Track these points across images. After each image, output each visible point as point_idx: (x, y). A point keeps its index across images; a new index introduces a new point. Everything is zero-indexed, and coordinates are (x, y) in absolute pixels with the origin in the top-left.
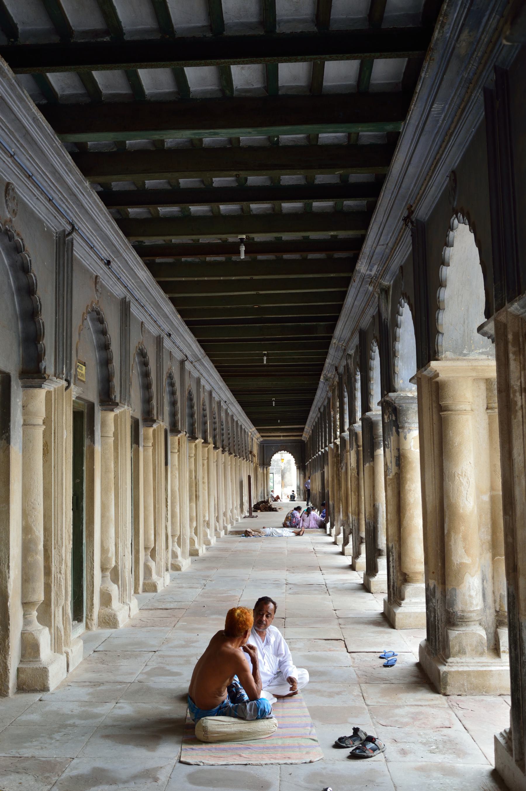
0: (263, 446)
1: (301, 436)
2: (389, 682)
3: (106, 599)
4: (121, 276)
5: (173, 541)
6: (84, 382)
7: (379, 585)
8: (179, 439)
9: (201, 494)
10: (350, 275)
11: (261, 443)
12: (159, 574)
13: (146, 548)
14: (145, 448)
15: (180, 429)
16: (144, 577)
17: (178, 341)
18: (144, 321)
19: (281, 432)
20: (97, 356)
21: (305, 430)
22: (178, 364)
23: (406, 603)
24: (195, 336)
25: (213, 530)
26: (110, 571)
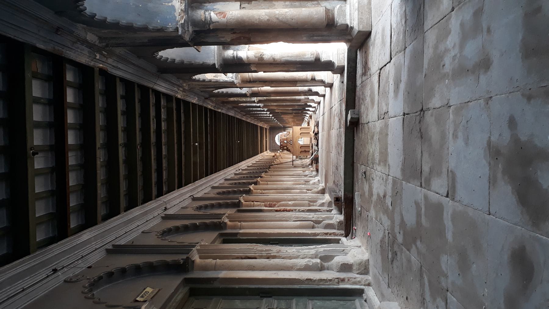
0: (272, 150)
1: (266, 129)
2: (422, 5)
3: (346, 267)
4: (81, 255)
5: (313, 206)
6: (159, 290)
7: (341, 59)
8: (246, 201)
9: (285, 186)
10: (191, 104)
11: (270, 151)
12: (331, 218)
13: (313, 227)
14: (241, 228)
15: (238, 201)
16: (334, 229)
17: (175, 202)
18: (141, 231)
19: (263, 139)
20: (147, 275)
21: (261, 126)
22: (194, 202)
23: (351, 23)
24: (175, 190)
25: (312, 178)
26: (324, 263)
